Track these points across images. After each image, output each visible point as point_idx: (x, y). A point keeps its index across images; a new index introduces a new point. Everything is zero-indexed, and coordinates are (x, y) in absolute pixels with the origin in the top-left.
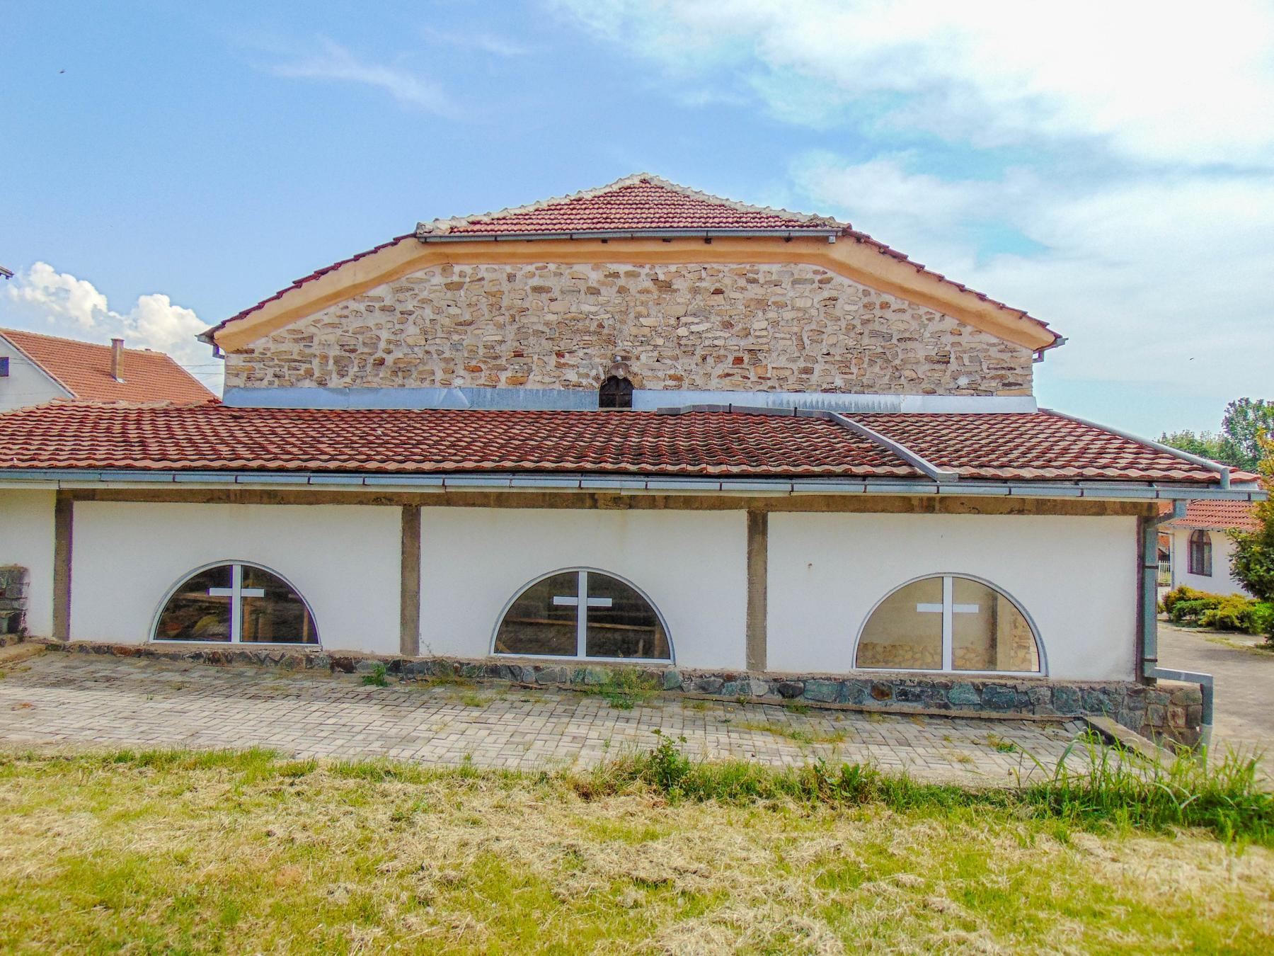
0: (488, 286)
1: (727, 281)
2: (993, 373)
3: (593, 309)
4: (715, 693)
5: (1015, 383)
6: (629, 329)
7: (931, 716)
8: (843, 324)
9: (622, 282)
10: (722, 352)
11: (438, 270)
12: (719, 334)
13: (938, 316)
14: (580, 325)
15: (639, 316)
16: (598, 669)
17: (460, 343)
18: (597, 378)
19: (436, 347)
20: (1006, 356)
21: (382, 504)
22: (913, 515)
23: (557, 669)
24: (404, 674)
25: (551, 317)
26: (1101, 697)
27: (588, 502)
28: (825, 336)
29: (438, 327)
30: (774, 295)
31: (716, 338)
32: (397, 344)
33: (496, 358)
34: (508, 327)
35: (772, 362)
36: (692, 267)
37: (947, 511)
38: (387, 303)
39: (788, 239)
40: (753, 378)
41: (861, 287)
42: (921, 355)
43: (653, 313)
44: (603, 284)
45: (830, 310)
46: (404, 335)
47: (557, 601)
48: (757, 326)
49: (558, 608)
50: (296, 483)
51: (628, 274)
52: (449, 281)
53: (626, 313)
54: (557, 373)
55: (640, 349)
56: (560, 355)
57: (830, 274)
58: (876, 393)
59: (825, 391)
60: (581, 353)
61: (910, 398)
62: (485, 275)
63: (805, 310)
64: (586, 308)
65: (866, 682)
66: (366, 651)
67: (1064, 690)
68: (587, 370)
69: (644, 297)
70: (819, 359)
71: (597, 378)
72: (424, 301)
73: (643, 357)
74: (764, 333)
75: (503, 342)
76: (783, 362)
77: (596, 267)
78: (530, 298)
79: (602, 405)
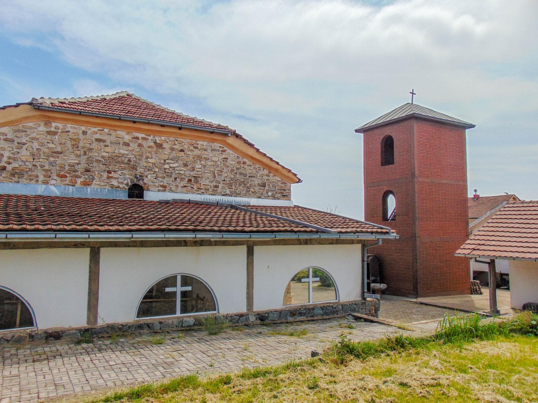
0: (71, 135)
1: (186, 147)
2: (279, 191)
3: (126, 152)
4: (239, 323)
5: (286, 196)
6: (143, 163)
7: (309, 321)
8: (230, 169)
9: (140, 141)
10: (183, 176)
11: (42, 124)
12: (182, 168)
13: (262, 169)
14: (120, 159)
15: (147, 158)
16: (188, 319)
17: (55, 162)
18: (127, 184)
19: (40, 163)
20: (283, 185)
21: (79, 247)
22: (300, 246)
23: (170, 322)
24: (92, 336)
25: (105, 154)
26: (355, 306)
27: (183, 244)
28: (223, 173)
29: (41, 153)
30: (205, 154)
31: (181, 170)
32: (15, 159)
33: (74, 171)
34: (82, 157)
35: (204, 182)
36: (171, 139)
37: (312, 244)
38: (9, 136)
39: (212, 133)
40: (195, 188)
41: (236, 155)
42: (256, 183)
43: (154, 156)
44: (131, 141)
45: (225, 163)
46: (19, 155)
47: (168, 290)
48: (197, 166)
49: (168, 293)
50: (228, 237)
51: (143, 138)
52: (49, 130)
53: (141, 156)
54: (107, 181)
55: (148, 172)
56: (109, 172)
57: (225, 148)
58: (241, 197)
59: (223, 195)
60: (120, 172)
61: (253, 199)
62: (70, 130)
63: (216, 162)
64: (122, 152)
65: (288, 311)
66: (66, 326)
67: (345, 305)
68: (123, 179)
69: (150, 150)
70: (221, 182)
71: (127, 184)
72: (33, 139)
73: (149, 176)
74: (200, 170)
75: (78, 164)
76: (207, 182)
77: (128, 133)
78: (94, 144)
79: (129, 196)
